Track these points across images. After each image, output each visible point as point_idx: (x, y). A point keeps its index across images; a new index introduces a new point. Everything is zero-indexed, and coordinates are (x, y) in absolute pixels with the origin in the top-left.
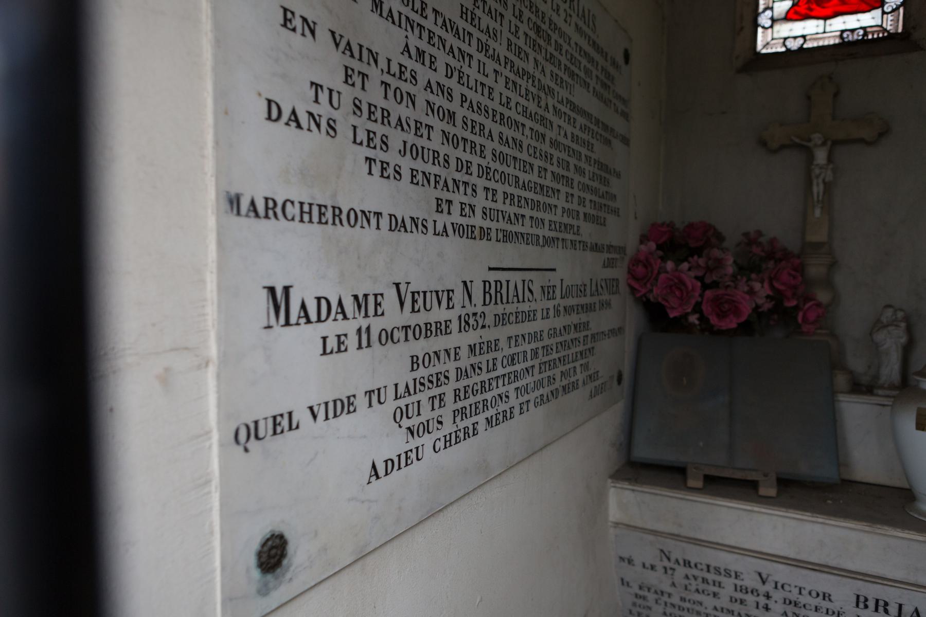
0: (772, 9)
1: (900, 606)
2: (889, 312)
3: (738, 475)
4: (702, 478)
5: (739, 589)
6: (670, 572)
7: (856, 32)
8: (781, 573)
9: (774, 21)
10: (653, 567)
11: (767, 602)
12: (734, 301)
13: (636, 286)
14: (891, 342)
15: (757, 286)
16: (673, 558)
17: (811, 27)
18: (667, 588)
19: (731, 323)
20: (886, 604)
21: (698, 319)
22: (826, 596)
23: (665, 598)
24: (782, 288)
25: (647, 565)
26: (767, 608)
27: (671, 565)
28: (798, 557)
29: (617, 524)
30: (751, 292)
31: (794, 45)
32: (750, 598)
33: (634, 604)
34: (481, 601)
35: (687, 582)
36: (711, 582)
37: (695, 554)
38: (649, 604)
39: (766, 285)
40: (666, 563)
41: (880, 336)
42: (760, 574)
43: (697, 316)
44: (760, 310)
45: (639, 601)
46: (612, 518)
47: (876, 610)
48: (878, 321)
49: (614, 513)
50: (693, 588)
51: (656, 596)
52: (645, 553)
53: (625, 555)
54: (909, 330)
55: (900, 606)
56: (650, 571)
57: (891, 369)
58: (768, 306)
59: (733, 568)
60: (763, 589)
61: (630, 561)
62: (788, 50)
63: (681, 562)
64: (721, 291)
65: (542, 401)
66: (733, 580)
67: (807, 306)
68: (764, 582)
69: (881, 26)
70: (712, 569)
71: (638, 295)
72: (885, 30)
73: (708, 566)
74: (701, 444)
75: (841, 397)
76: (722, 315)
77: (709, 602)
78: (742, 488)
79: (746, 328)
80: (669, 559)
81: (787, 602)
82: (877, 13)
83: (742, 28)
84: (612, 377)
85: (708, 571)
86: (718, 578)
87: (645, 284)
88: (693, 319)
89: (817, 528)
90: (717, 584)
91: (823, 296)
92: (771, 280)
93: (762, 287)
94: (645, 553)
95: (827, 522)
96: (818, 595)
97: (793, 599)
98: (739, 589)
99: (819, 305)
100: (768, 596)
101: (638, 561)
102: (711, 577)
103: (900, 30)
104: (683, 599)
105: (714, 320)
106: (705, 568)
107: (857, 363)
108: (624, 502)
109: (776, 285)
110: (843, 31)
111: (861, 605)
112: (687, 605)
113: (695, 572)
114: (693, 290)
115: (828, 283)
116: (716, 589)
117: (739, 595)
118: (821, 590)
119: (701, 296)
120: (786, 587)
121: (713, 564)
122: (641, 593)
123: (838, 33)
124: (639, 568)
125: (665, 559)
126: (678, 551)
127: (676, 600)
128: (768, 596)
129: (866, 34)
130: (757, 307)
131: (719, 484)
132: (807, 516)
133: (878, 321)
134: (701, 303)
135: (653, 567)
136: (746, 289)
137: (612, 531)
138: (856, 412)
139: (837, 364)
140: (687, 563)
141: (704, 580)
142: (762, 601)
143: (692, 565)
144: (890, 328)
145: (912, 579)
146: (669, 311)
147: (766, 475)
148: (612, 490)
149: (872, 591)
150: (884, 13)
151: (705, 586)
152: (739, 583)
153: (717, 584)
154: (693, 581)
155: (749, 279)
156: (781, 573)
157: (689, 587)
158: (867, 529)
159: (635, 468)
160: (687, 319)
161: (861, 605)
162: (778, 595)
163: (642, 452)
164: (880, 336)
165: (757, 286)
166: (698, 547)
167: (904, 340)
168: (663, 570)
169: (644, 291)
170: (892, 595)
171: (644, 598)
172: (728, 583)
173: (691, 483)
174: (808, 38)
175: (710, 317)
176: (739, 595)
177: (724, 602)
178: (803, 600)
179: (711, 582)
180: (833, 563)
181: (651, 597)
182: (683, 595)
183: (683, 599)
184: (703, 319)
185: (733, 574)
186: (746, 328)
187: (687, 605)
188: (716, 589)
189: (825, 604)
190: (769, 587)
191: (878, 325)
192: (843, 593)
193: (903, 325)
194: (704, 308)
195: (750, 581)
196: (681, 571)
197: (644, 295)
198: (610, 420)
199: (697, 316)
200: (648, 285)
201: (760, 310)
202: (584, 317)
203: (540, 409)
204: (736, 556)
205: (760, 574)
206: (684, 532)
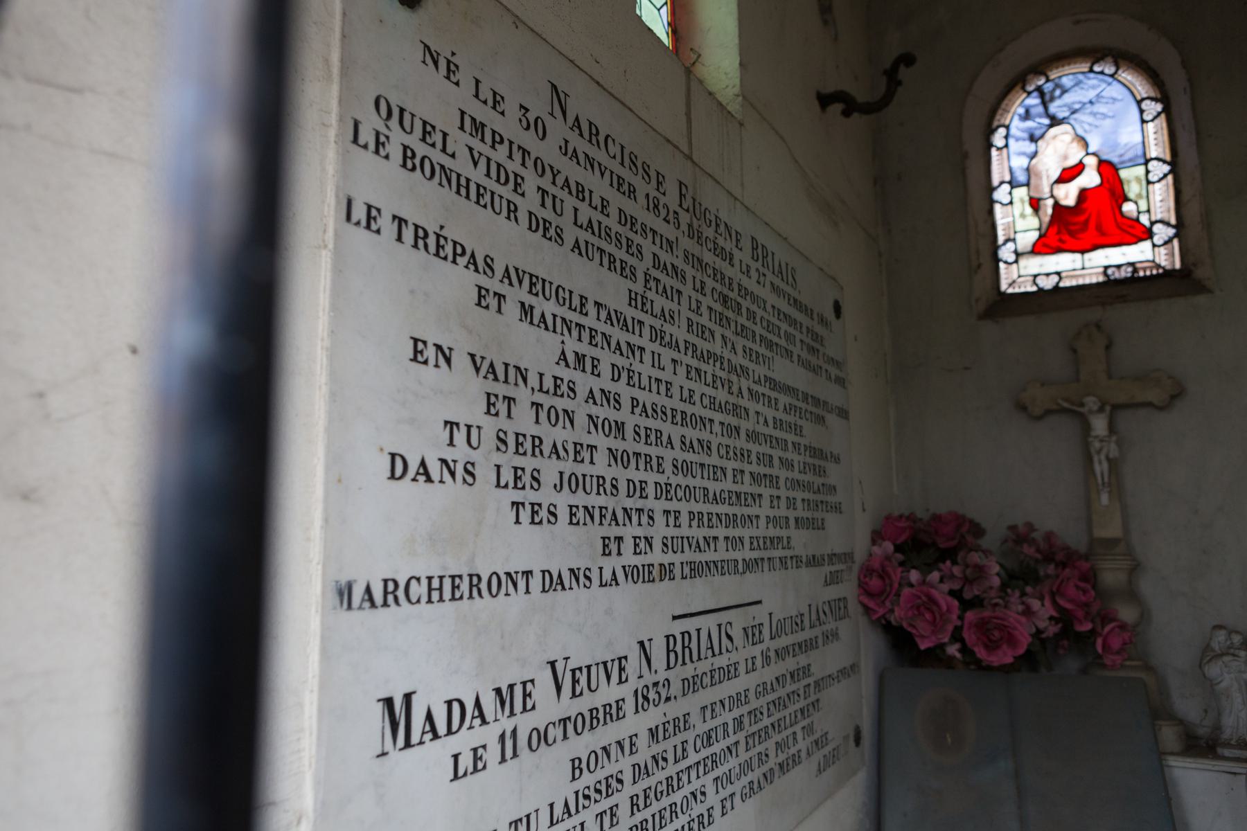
0: (1014, 240)
7: (1123, 268)
9: (1018, 255)
13: (871, 605)
15: (1035, 604)
17: (1065, 262)
19: (1005, 656)
21: (960, 651)
24: (1068, 606)
30: (1028, 612)
31: (1047, 284)
39: (1047, 602)
44: (1044, 636)
48: (1207, 648)
62: (1041, 290)
67: (1107, 629)
69: (1153, 261)
71: (875, 617)
72: (1158, 266)
76: (992, 646)
82: (1146, 246)
83: (979, 266)
84: (846, 738)
87: (883, 602)
88: (953, 650)
91: (1127, 614)
93: (1043, 605)
103: (1178, 265)
109: (1061, 602)
110: (1106, 268)
114: (949, 610)
115: (1132, 595)
123: (1101, 270)
129: (1135, 270)
133: (1207, 648)
134: (962, 627)
139: (1160, 712)
146: (917, 639)
150: (1154, 246)
165: (1035, 604)
174: (1063, 275)
175: (976, 649)
194: (965, 635)
200: (888, 604)
201: (1044, 636)
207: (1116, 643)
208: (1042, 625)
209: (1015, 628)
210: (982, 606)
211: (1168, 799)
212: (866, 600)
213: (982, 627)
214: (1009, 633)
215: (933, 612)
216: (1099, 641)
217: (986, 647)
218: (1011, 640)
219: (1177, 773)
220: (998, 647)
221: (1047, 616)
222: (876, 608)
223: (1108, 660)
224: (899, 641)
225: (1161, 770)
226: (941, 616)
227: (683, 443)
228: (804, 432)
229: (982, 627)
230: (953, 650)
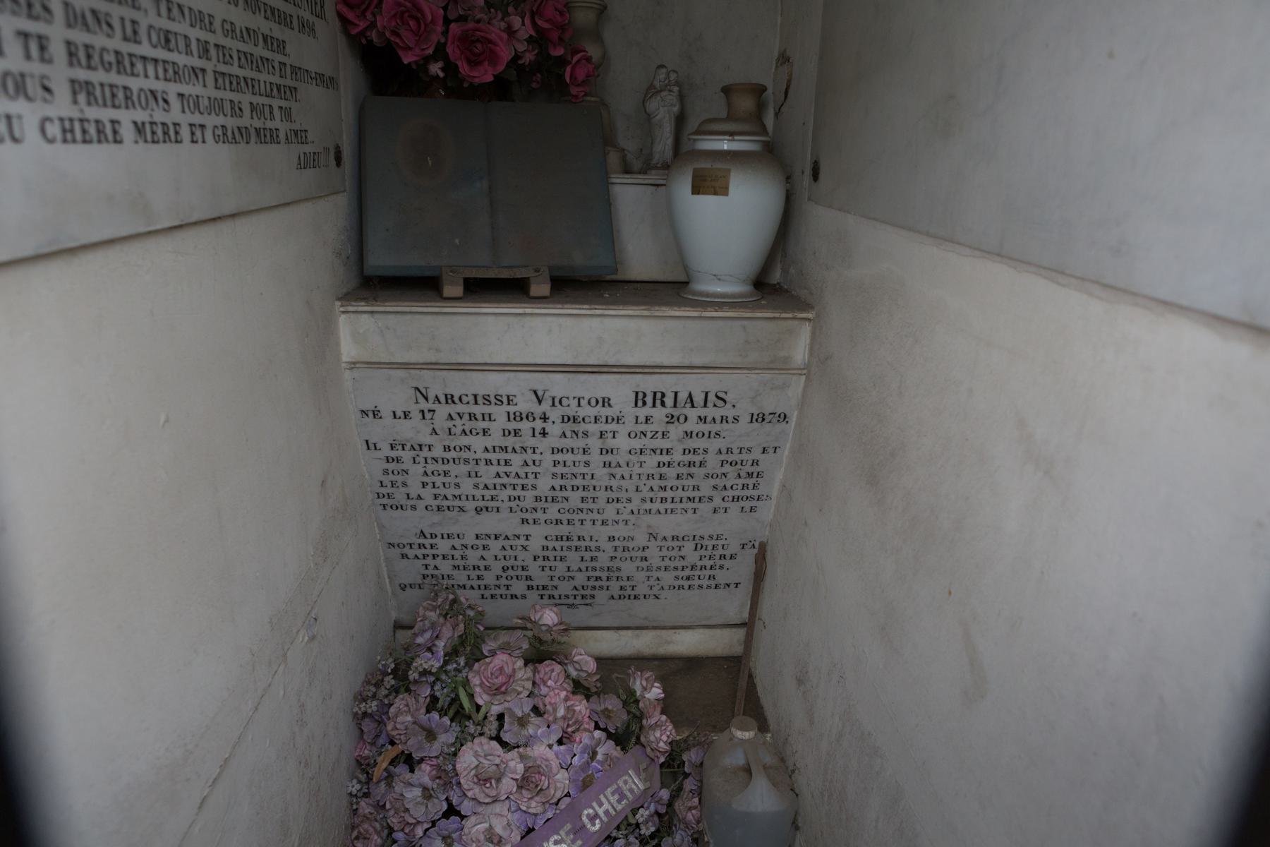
1: (676, 394)
2: (662, 74)
3: (505, 274)
4: (461, 282)
5: (512, 416)
6: (428, 416)
8: (558, 385)
10: (406, 415)
11: (544, 425)
12: (490, 42)
13: (350, 16)
14: (663, 110)
15: (516, 21)
16: (431, 397)
18: (428, 439)
19: (485, 75)
20: (663, 395)
21: (443, 69)
22: (606, 402)
23: (425, 453)
24: (546, 26)
25: (400, 414)
26: (544, 433)
27: (431, 406)
28: (577, 362)
29: (353, 365)
30: (510, 31)
32: (525, 426)
33: (386, 472)
34: (167, 421)
35: (450, 424)
36: (479, 417)
37: (458, 384)
38: (404, 467)
39: (527, 21)
40: (424, 405)
41: (653, 105)
42: (535, 392)
43: (440, 64)
44: (520, 62)
45: (391, 466)
46: (345, 359)
47: (654, 405)
48: (651, 86)
49: (348, 350)
50: (458, 430)
51: (413, 453)
52: (394, 395)
53: (369, 406)
54: (681, 97)
55: (676, 394)
56: (402, 421)
57: (663, 145)
58: (529, 58)
59: (503, 392)
60: (538, 410)
61: (376, 414)
63: (443, 399)
64: (471, 25)
65: (223, 136)
66: (505, 408)
67: (575, 59)
68: (540, 402)
70: (480, 400)
71: (354, 32)
73: (475, 396)
74: (457, 241)
75: (616, 178)
76: (474, 63)
77: (478, 443)
78: (511, 288)
79: (500, 89)
80: (426, 399)
81: (567, 419)
84: (326, 149)
85: (476, 403)
86: (487, 409)
87: (364, 12)
88: (436, 69)
89: (595, 322)
90: (487, 418)
91: (593, 51)
92: (533, 15)
93: (523, 24)
94: (394, 395)
95: (607, 312)
96: (597, 402)
97: (571, 414)
98: (512, 416)
99: (589, 59)
100: (545, 418)
101: (386, 412)
102: (478, 410)
104: (447, 449)
105: (464, 68)
106: (471, 399)
107: (629, 143)
108: (364, 332)
109: (540, 23)
111: (640, 403)
112: (453, 454)
113: (460, 408)
114: (433, 21)
115: (598, 37)
116: (485, 425)
117: (513, 425)
118: (599, 395)
119: (445, 33)
120: (565, 402)
121: (481, 392)
122: (393, 454)
124: (388, 419)
125: (421, 399)
126: (436, 384)
127: (438, 452)
128: (545, 418)
130: (517, 57)
131: (482, 288)
132: (584, 310)
133: (651, 86)
134: (445, 44)
135: (406, 415)
136: (503, 25)
137: (347, 375)
138: (629, 197)
139: (609, 141)
140: (450, 399)
141: (472, 417)
142: (539, 424)
143: (456, 399)
144: (664, 94)
145: (687, 363)
146: (400, 53)
147: (537, 270)
148: (343, 316)
149: (650, 384)
151: (473, 424)
152: (512, 409)
153: (487, 418)
154: (458, 422)
155: (506, 14)
156: (558, 385)
157: (453, 430)
158: (646, 313)
159: (375, 284)
160: (426, 71)
161: (640, 403)
162: (554, 415)
163: (381, 260)
164: (653, 105)
165: (516, 21)
166: (462, 373)
167: (676, 109)
168: (420, 416)
169: (363, 25)
170: (666, 383)
171: (398, 460)
172: (499, 412)
173: (448, 291)
175: (459, 64)
176: (513, 425)
177: (496, 439)
178: (582, 413)
179: (479, 417)
180: (611, 361)
181: (407, 455)
182: (447, 443)
183: (447, 449)
184: (450, 68)
185: (505, 400)
186: (500, 89)
187: (453, 454)
188: (485, 425)
189: (606, 411)
190: (546, 406)
191: (651, 91)
192: (620, 391)
193: (676, 89)
194: (449, 50)
195: (525, 404)
196: (443, 410)
197: (362, 33)
198: (331, 214)
199: (440, 64)
200: (369, 16)
201: (520, 62)
202: (277, 31)
203: (224, 149)
204: (507, 374)
205: (535, 392)
206: (444, 357)
207: (581, 75)
208: (521, 47)
209: (495, 44)
210: (466, 20)
211: (608, 200)
212: (344, 10)
213: (466, 41)
214: (491, 51)
215: (417, 20)
216: (568, 69)
217: (469, 62)
218: (493, 58)
219: (617, 190)
220: (480, 63)
221: (527, 36)
222: (356, 21)
223: (574, 90)
224: (385, 71)
225: (607, 184)
226: (426, 25)
227: (166, 101)
228: (288, 50)
229: (466, 41)
230: (436, 69)
